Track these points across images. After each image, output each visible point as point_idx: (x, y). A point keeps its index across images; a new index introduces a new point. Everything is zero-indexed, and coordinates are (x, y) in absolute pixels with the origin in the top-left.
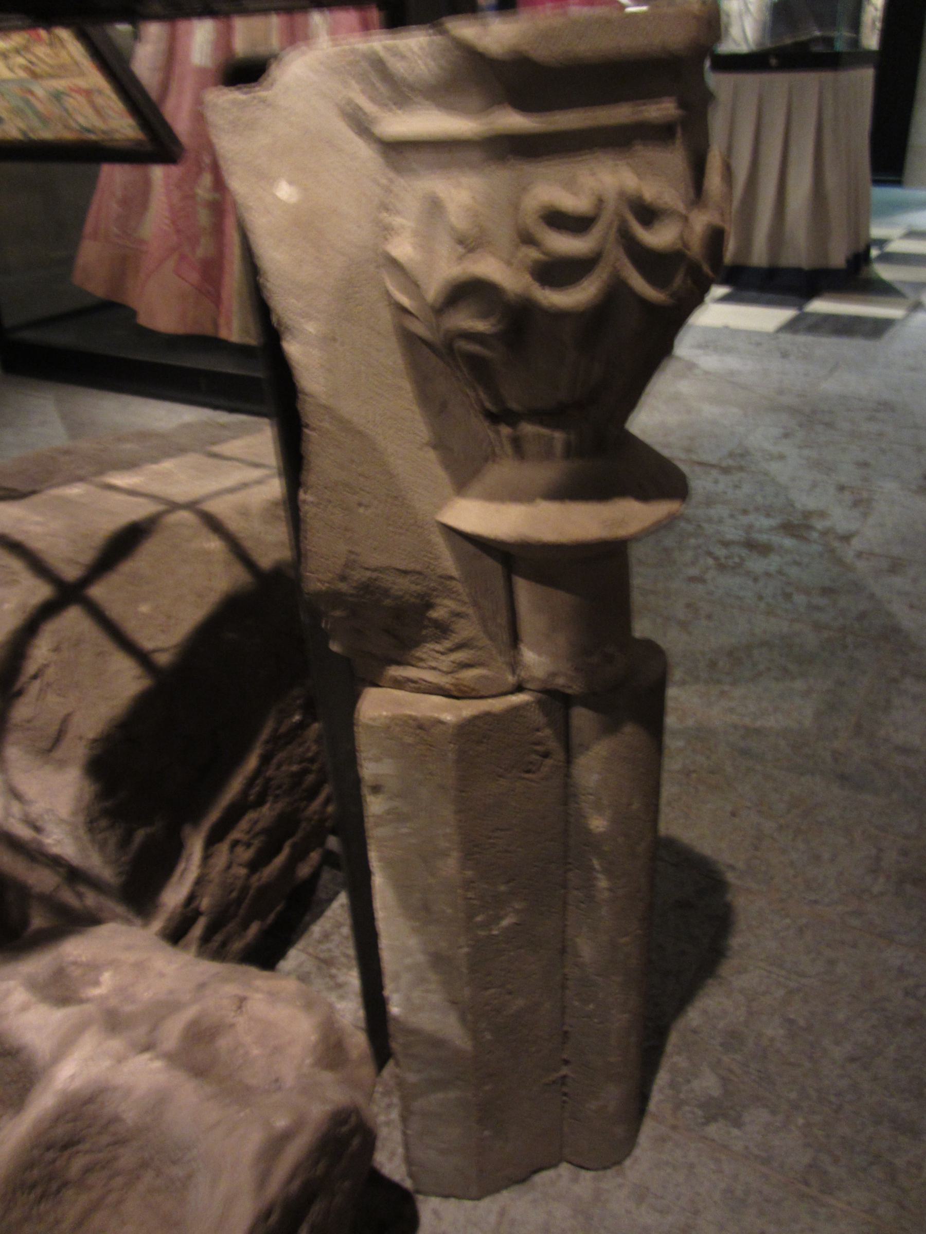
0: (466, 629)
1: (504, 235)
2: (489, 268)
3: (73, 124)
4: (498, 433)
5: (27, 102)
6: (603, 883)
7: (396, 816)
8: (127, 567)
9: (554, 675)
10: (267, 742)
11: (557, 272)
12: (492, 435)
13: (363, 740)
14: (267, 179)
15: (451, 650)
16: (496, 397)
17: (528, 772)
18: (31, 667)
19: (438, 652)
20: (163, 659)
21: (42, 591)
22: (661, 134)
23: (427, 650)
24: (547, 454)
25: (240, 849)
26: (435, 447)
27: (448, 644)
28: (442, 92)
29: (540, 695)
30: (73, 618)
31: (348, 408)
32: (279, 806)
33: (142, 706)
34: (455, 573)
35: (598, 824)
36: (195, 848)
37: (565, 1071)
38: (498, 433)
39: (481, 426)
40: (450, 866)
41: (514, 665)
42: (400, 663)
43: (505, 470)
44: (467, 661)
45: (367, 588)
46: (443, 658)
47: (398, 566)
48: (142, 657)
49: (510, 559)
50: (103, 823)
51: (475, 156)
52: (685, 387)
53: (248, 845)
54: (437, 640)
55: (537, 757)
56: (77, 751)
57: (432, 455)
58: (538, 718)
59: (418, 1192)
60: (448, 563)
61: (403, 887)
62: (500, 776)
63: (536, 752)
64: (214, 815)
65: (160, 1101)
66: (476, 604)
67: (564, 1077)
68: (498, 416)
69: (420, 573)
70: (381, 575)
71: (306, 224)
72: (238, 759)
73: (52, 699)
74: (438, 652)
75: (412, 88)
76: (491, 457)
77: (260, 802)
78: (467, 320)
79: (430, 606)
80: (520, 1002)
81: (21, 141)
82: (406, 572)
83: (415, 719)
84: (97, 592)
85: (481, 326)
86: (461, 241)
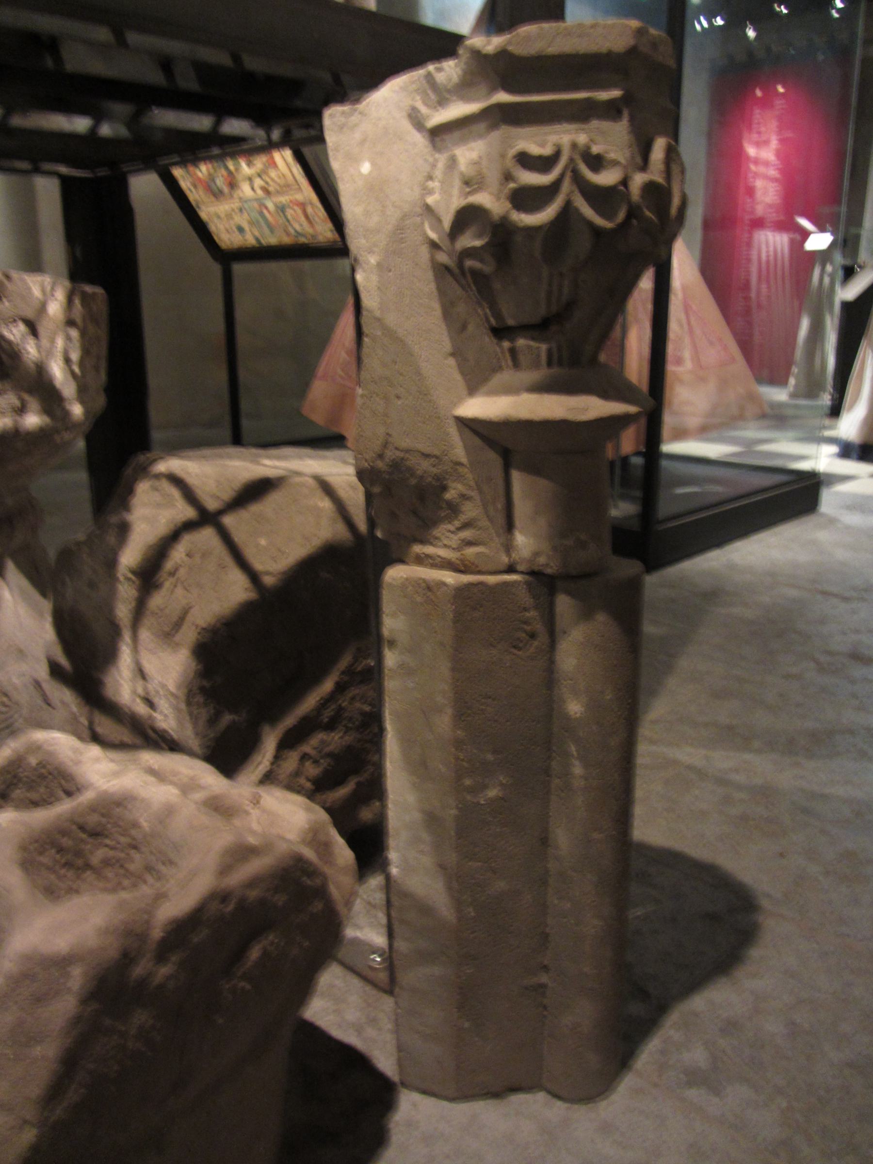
0: (470, 511)
1: (493, 177)
2: (483, 199)
3: (292, 231)
4: (501, 347)
5: (261, 214)
6: (578, 770)
7: (406, 670)
8: (255, 508)
9: (536, 554)
10: (343, 673)
11: (526, 199)
12: (498, 349)
13: (386, 597)
14: (353, 159)
15: (459, 529)
16: (498, 315)
17: (515, 647)
18: (169, 565)
19: (450, 531)
20: (268, 581)
21: (189, 513)
22: (611, 110)
23: (442, 530)
24: (536, 365)
25: (308, 764)
26: (453, 354)
27: (457, 523)
28: (464, 88)
29: (527, 577)
30: (207, 536)
31: (391, 319)
32: (349, 739)
33: (246, 611)
34: (464, 460)
35: (575, 708)
36: (270, 744)
37: (544, 979)
38: (501, 347)
39: (488, 340)
40: (444, 722)
41: (508, 547)
42: (423, 542)
43: (506, 376)
44: (471, 539)
45: (396, 465)
46: (452, 536)
47: (423, 450)
48: (254, 577)
49: (502, 442)
50: (200, 699)
51: (482, 126)
52: (823, 536)
53: (316, 762)
54: (449, 519)
55: (524, 635)
56: (189, 635)
57: (452, 361)
58: (524, 598)
59: (403, 1084)
60: (459, 452)
61: (407, 741)
62: (491, 645)
63: (525, 631)
64: (289, 721)
65: (169, 811)
66: (480, 491)
67: (543, 986)
68: (500, 332)
69: (436, 457)
70: (407, 455)
71: (375, 188)
72: (316, 679)
73: (179, 591)
74: (450, 531)
75: (449, 91)
76: (497, 369)
77: (330, 726)
78: (470, 240)
79: (444, 488)
80: (501, 885)
81: (254, 247)
82: (427, 456)
83: (424, 581)
84: (228, 520)
85: (478, 243)
86: (467, 183)
